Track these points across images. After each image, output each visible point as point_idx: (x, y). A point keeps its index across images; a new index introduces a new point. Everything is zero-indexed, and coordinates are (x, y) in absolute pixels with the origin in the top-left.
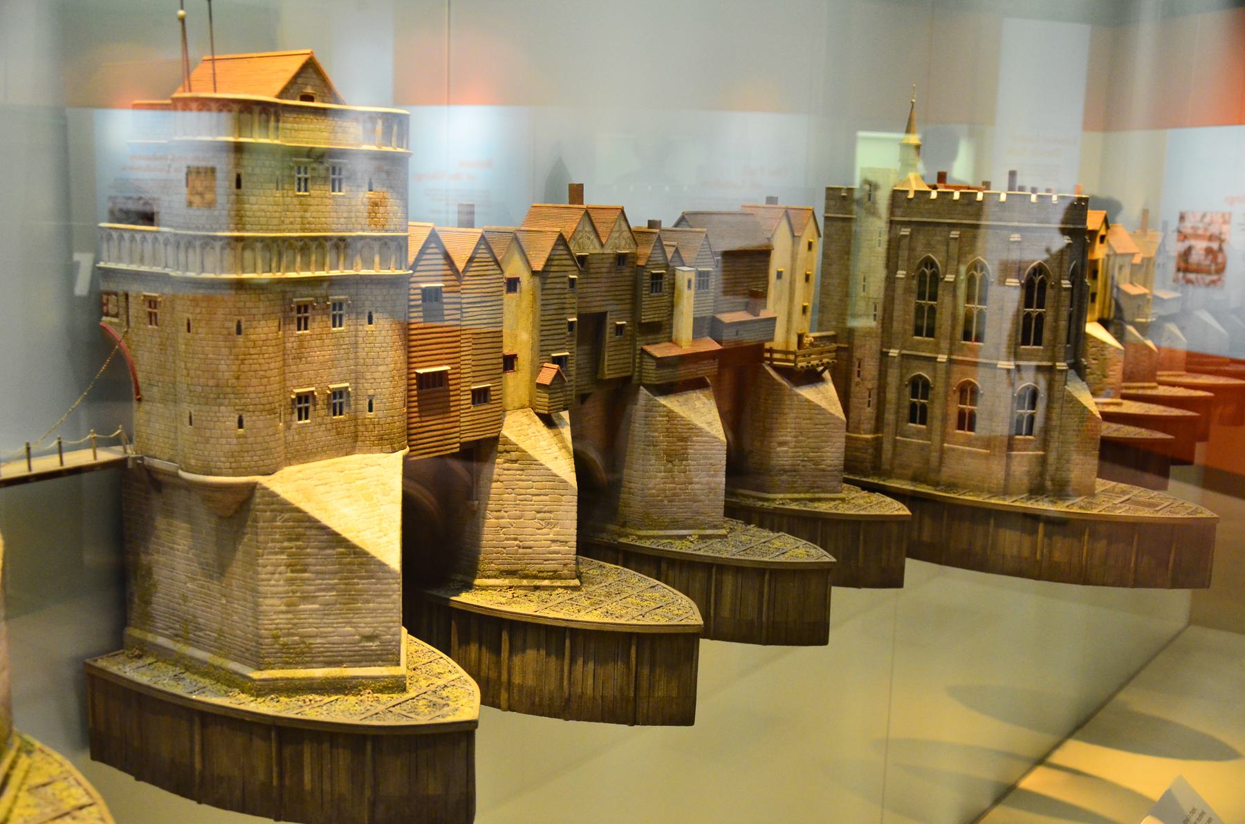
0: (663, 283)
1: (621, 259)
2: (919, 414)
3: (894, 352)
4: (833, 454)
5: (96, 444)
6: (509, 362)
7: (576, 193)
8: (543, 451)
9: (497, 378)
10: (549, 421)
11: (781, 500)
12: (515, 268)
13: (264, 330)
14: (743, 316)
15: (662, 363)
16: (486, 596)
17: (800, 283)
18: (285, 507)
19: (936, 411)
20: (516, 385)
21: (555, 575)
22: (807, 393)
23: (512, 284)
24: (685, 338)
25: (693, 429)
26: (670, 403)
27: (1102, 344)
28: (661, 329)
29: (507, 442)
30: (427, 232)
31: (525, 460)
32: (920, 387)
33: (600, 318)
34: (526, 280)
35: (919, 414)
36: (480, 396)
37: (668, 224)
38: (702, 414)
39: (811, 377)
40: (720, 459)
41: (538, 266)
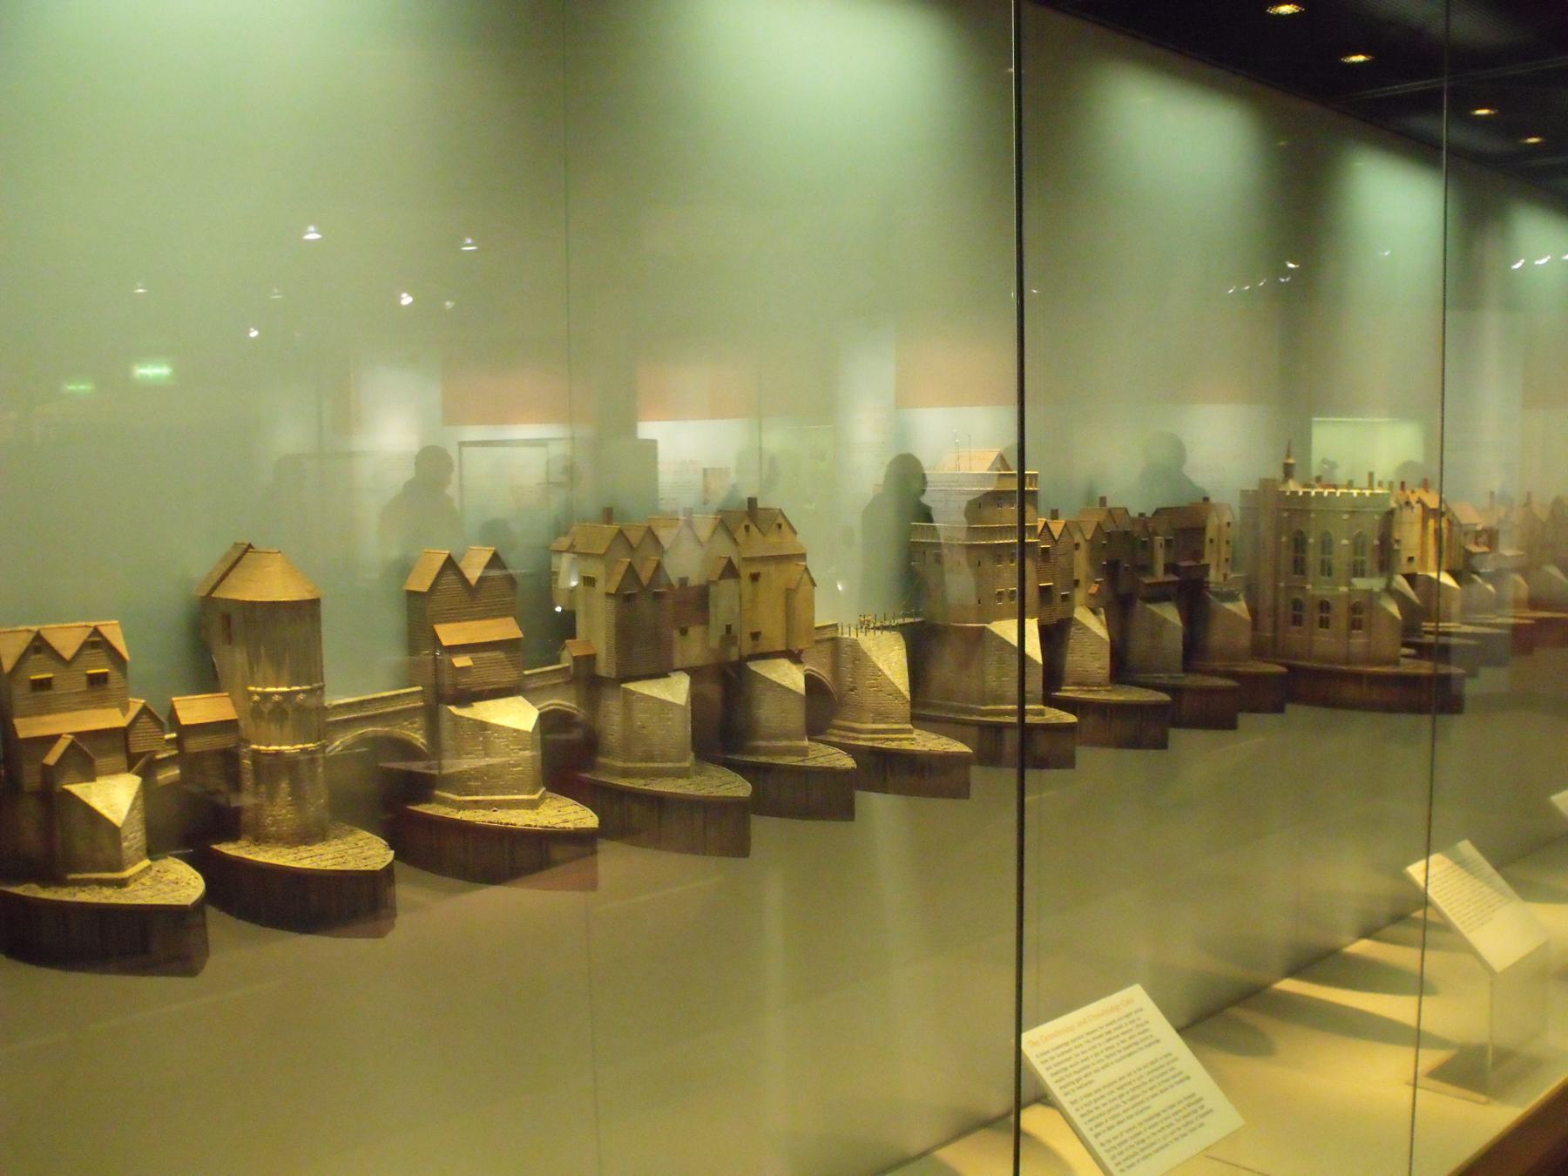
0: (1147, 546)
1: (1127, 533)
2: (1297, 621)
3: (1282, 584)
4: (1244, 640)
5: (905, 616)
6: (1077, 583)
7: (1103, 501)
8: (1093, 624)
9: (1072, 590)
10: (1094, 612)
11: (1217, 664)
12: (1078, 538)
13: (988, 564)
14: (1191, 563)
15: (1149, 585)
16: (1068, 692)
17: (1223, 544)
18: (997, 637)
19: (1306, 616)
20: (1080, 595)
21: (1100, 685)
22: (1229, 606)
23: (1077, 546)
24: (1160, 575)
25: (1165, 621)
26: (1154, 608)
27: (1448, 588)
28: (1147, 569)
29: (1079, 623)
30: (443, 558)
31: (1085, 629)
32: (1297, 605)
33: (1117, 562)
34: (1083, 545)
35: (1297, 621)
36: (1065, 598)
37: (1149, 515)
38: (1170, 614)
39: (1231, 597)
40: (1179, 636)
41: (1088, 537)
